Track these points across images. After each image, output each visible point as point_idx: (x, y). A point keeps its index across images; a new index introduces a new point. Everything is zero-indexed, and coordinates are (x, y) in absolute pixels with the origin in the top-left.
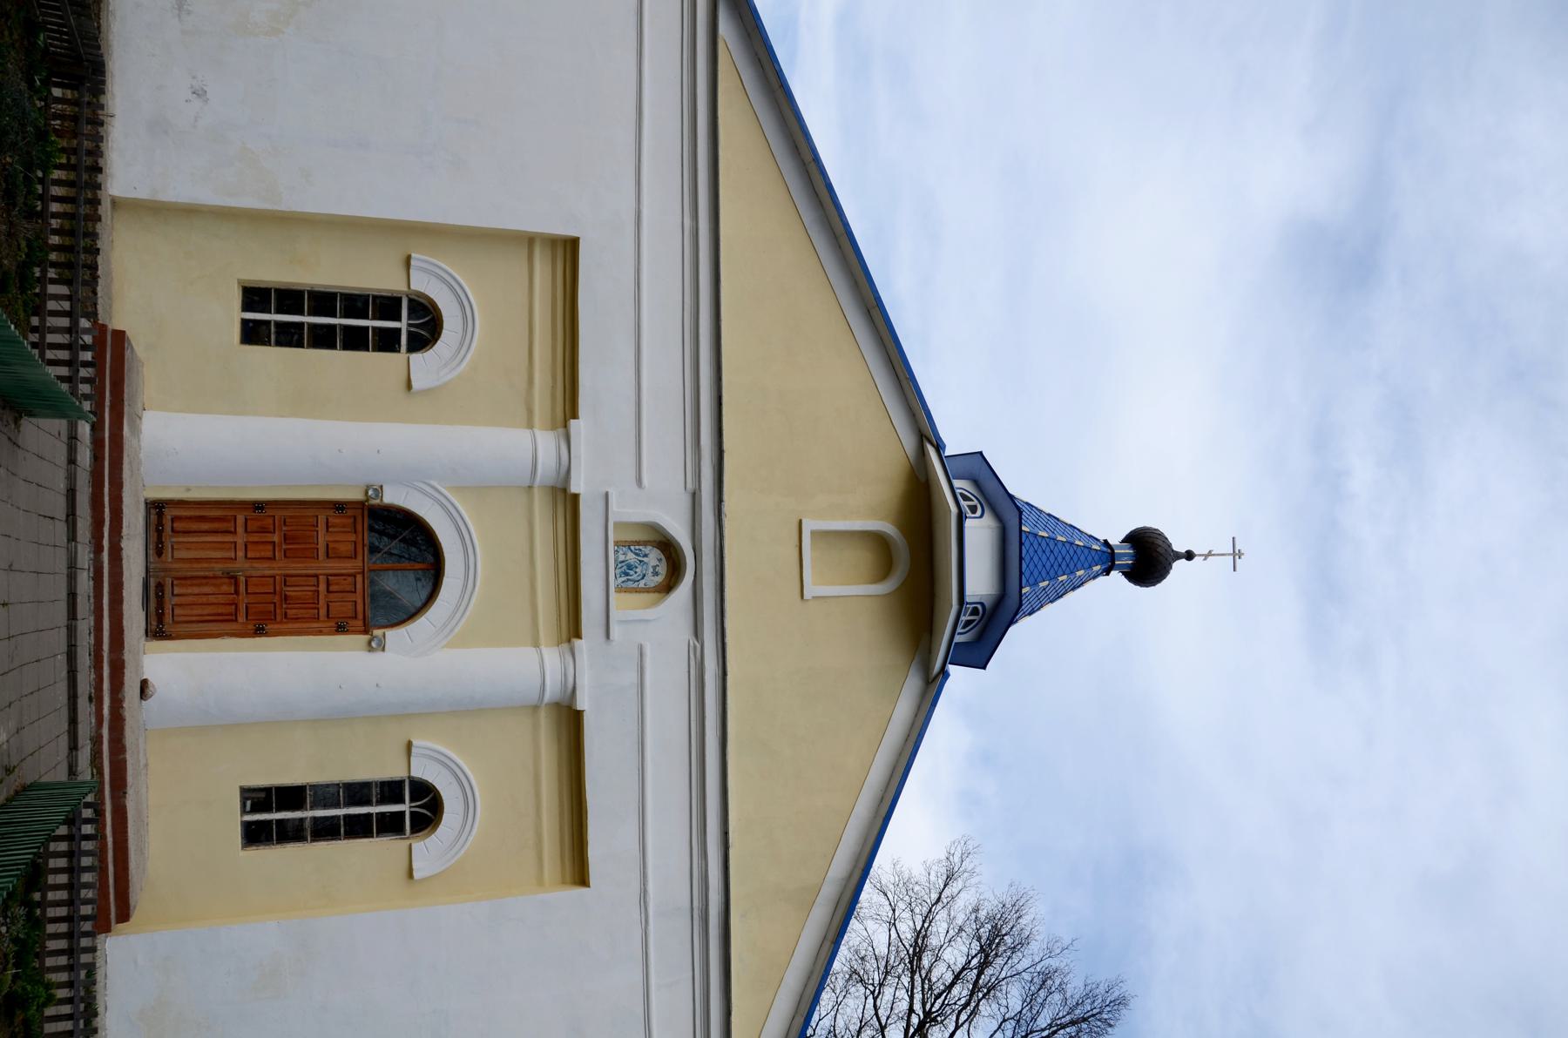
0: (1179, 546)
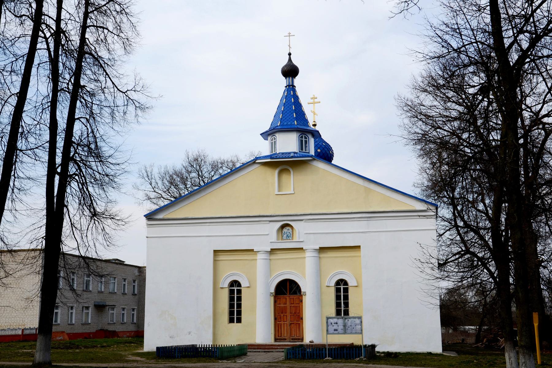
0: (285, 62)
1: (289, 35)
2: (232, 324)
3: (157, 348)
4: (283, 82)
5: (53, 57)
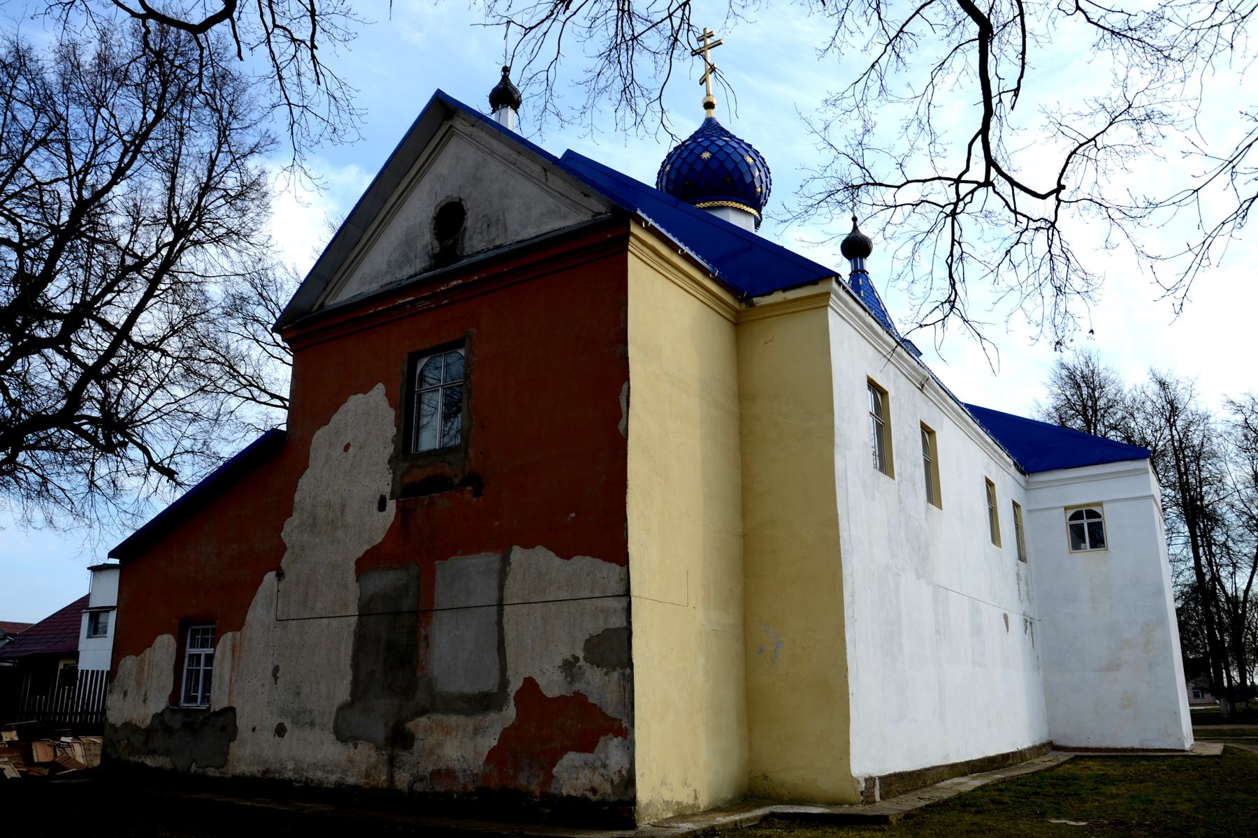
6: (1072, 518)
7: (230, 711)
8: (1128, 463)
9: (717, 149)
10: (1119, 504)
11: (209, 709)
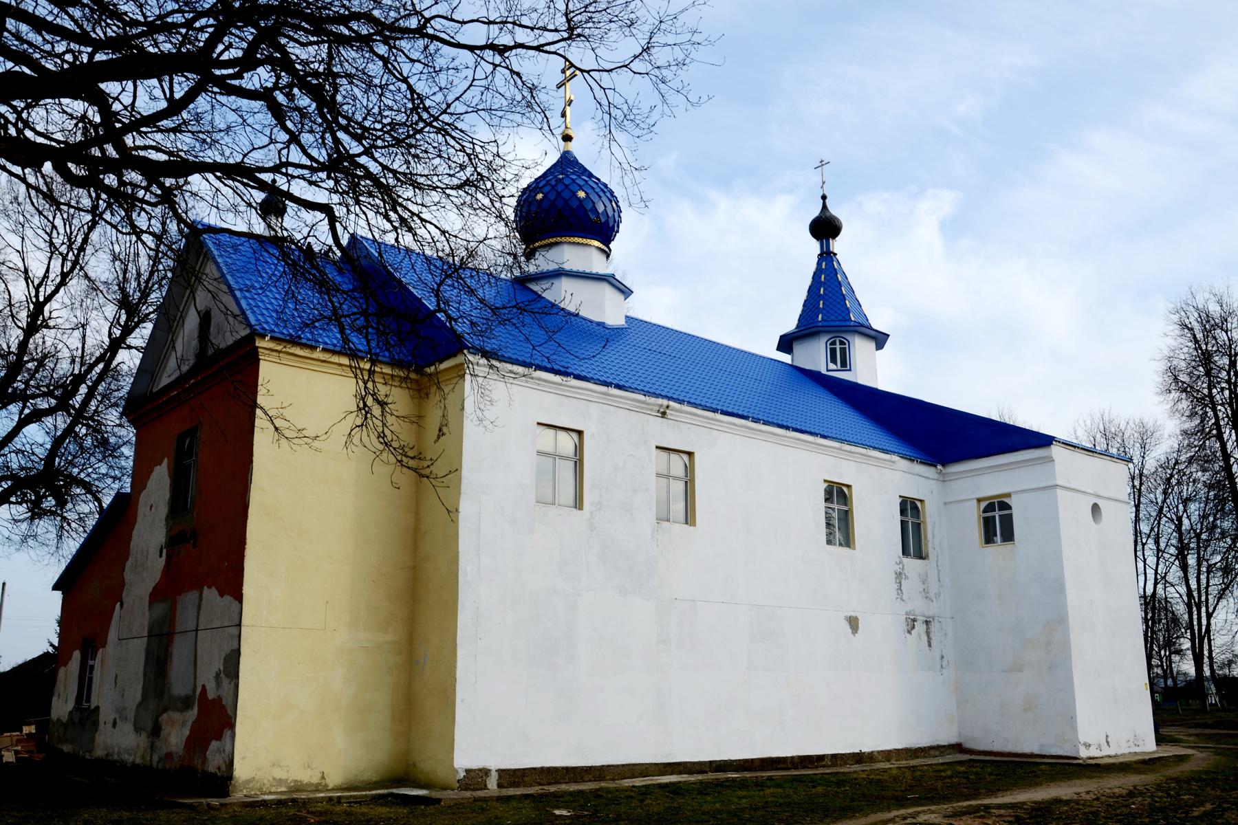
0: (816, 212)
1: (822, 164)
2: (991, 549)
3: (222, 596)
4: (814, 247)
5: (229, 81)
6: (985, 511)
7: (97, 708)
8: (1032, 451)
9: (571, 181)
10: (1027, 495)
11: (89, 706)
